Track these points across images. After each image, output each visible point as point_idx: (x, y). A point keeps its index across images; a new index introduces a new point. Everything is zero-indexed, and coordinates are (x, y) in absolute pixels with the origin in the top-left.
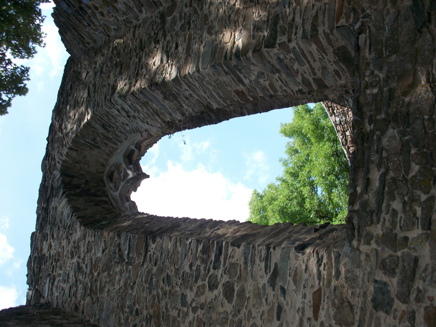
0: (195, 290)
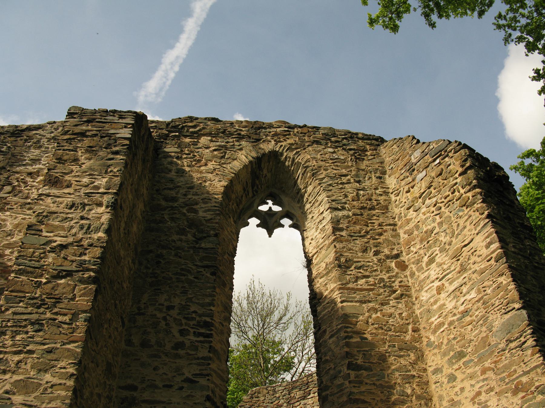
0: (178, 317)
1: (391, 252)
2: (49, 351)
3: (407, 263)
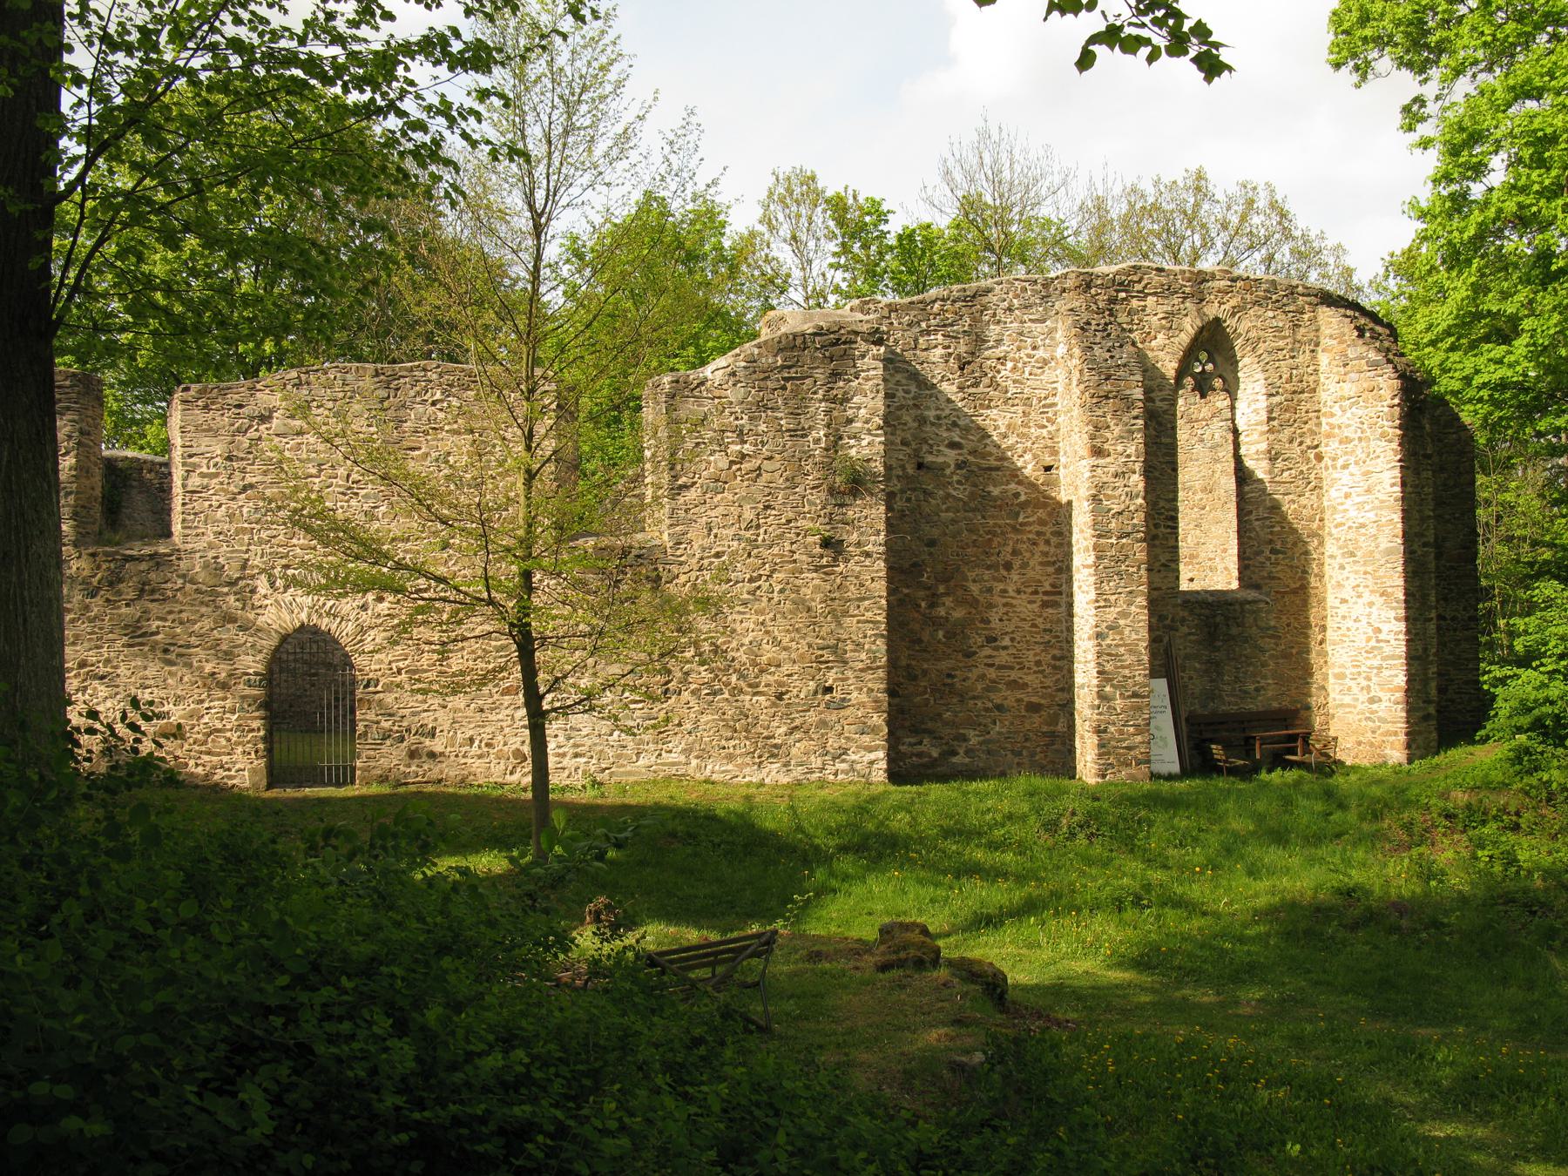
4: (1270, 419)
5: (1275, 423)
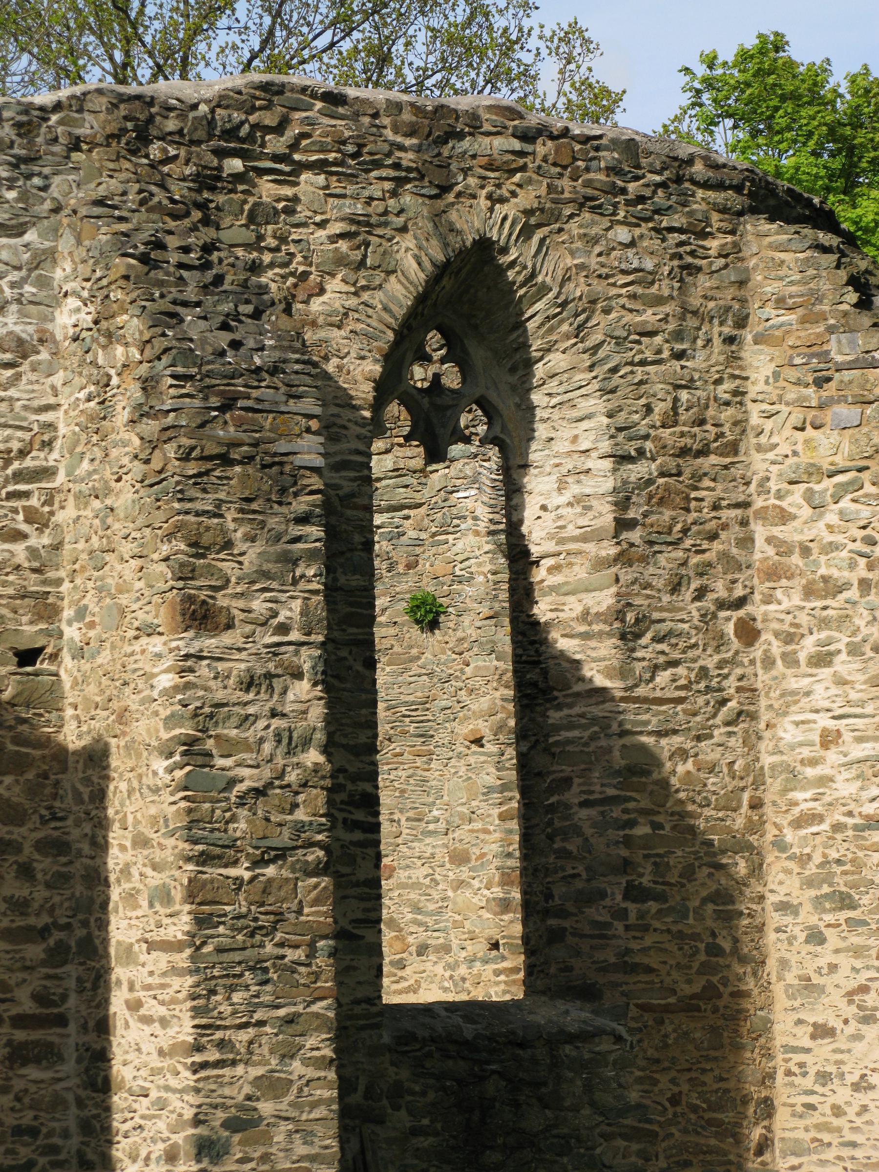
1: (730, 590)
2: (290, 1020)
3: (759, 625)
4: (623, 525)
5: (635, 536)
